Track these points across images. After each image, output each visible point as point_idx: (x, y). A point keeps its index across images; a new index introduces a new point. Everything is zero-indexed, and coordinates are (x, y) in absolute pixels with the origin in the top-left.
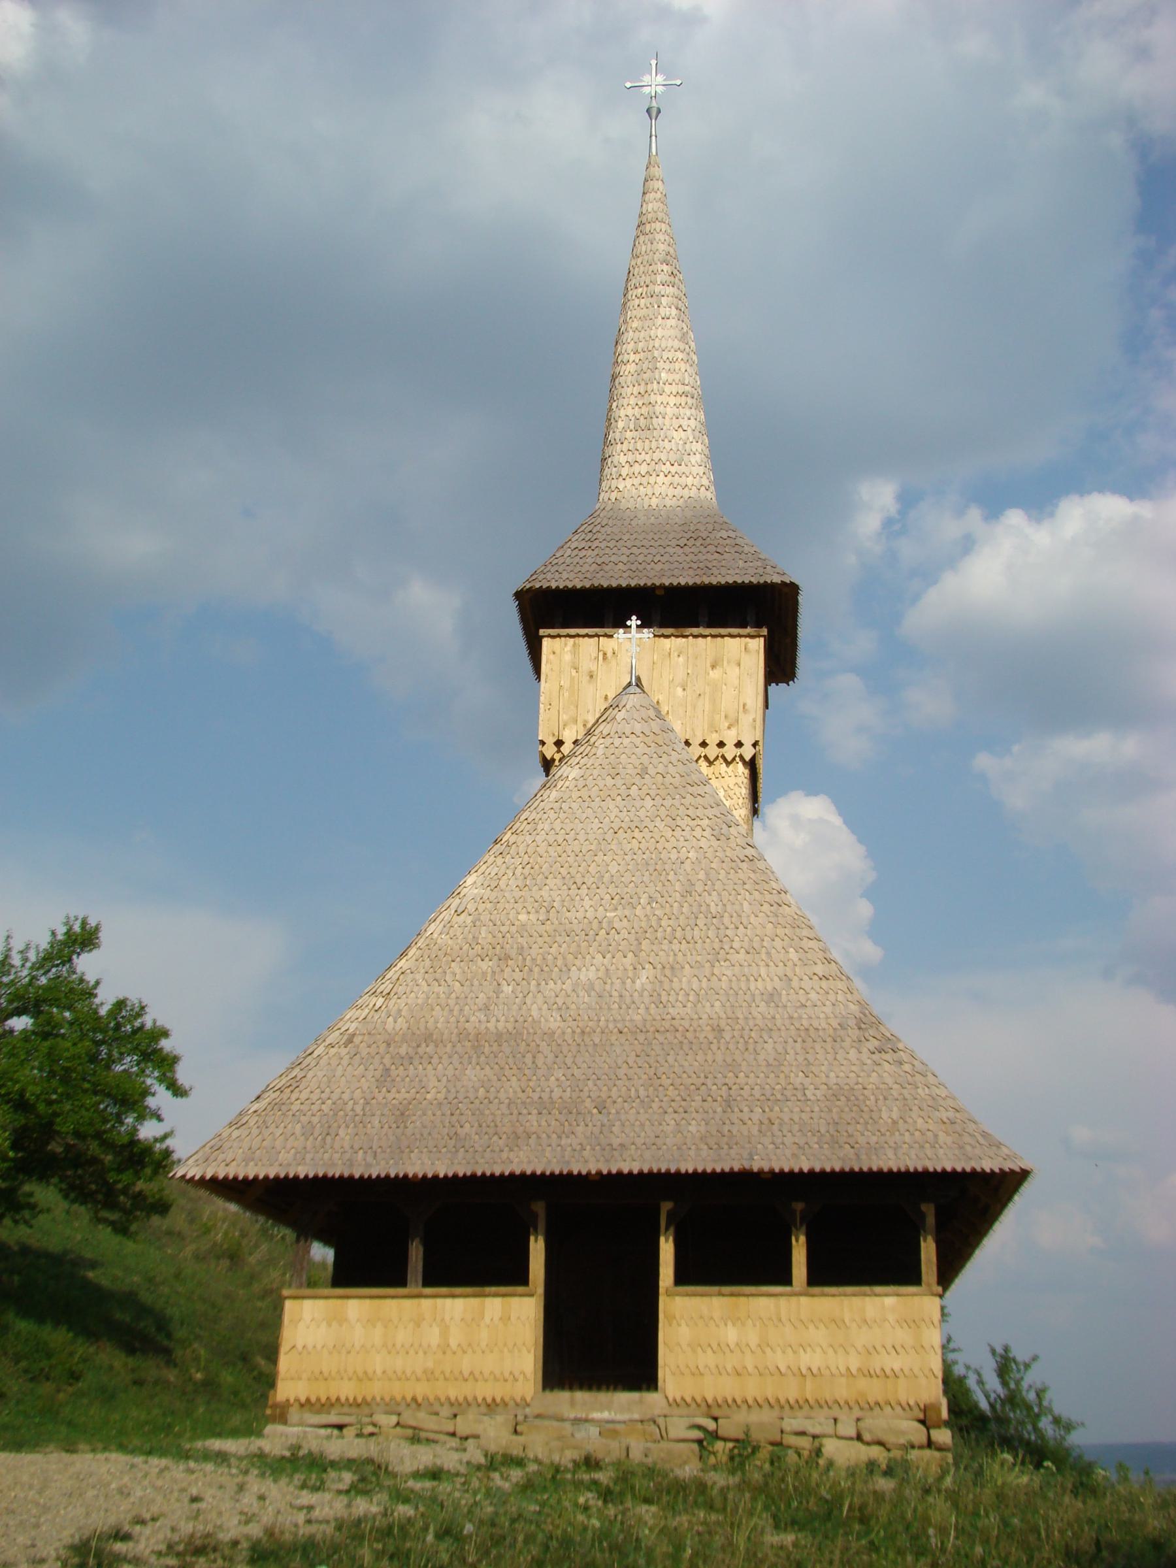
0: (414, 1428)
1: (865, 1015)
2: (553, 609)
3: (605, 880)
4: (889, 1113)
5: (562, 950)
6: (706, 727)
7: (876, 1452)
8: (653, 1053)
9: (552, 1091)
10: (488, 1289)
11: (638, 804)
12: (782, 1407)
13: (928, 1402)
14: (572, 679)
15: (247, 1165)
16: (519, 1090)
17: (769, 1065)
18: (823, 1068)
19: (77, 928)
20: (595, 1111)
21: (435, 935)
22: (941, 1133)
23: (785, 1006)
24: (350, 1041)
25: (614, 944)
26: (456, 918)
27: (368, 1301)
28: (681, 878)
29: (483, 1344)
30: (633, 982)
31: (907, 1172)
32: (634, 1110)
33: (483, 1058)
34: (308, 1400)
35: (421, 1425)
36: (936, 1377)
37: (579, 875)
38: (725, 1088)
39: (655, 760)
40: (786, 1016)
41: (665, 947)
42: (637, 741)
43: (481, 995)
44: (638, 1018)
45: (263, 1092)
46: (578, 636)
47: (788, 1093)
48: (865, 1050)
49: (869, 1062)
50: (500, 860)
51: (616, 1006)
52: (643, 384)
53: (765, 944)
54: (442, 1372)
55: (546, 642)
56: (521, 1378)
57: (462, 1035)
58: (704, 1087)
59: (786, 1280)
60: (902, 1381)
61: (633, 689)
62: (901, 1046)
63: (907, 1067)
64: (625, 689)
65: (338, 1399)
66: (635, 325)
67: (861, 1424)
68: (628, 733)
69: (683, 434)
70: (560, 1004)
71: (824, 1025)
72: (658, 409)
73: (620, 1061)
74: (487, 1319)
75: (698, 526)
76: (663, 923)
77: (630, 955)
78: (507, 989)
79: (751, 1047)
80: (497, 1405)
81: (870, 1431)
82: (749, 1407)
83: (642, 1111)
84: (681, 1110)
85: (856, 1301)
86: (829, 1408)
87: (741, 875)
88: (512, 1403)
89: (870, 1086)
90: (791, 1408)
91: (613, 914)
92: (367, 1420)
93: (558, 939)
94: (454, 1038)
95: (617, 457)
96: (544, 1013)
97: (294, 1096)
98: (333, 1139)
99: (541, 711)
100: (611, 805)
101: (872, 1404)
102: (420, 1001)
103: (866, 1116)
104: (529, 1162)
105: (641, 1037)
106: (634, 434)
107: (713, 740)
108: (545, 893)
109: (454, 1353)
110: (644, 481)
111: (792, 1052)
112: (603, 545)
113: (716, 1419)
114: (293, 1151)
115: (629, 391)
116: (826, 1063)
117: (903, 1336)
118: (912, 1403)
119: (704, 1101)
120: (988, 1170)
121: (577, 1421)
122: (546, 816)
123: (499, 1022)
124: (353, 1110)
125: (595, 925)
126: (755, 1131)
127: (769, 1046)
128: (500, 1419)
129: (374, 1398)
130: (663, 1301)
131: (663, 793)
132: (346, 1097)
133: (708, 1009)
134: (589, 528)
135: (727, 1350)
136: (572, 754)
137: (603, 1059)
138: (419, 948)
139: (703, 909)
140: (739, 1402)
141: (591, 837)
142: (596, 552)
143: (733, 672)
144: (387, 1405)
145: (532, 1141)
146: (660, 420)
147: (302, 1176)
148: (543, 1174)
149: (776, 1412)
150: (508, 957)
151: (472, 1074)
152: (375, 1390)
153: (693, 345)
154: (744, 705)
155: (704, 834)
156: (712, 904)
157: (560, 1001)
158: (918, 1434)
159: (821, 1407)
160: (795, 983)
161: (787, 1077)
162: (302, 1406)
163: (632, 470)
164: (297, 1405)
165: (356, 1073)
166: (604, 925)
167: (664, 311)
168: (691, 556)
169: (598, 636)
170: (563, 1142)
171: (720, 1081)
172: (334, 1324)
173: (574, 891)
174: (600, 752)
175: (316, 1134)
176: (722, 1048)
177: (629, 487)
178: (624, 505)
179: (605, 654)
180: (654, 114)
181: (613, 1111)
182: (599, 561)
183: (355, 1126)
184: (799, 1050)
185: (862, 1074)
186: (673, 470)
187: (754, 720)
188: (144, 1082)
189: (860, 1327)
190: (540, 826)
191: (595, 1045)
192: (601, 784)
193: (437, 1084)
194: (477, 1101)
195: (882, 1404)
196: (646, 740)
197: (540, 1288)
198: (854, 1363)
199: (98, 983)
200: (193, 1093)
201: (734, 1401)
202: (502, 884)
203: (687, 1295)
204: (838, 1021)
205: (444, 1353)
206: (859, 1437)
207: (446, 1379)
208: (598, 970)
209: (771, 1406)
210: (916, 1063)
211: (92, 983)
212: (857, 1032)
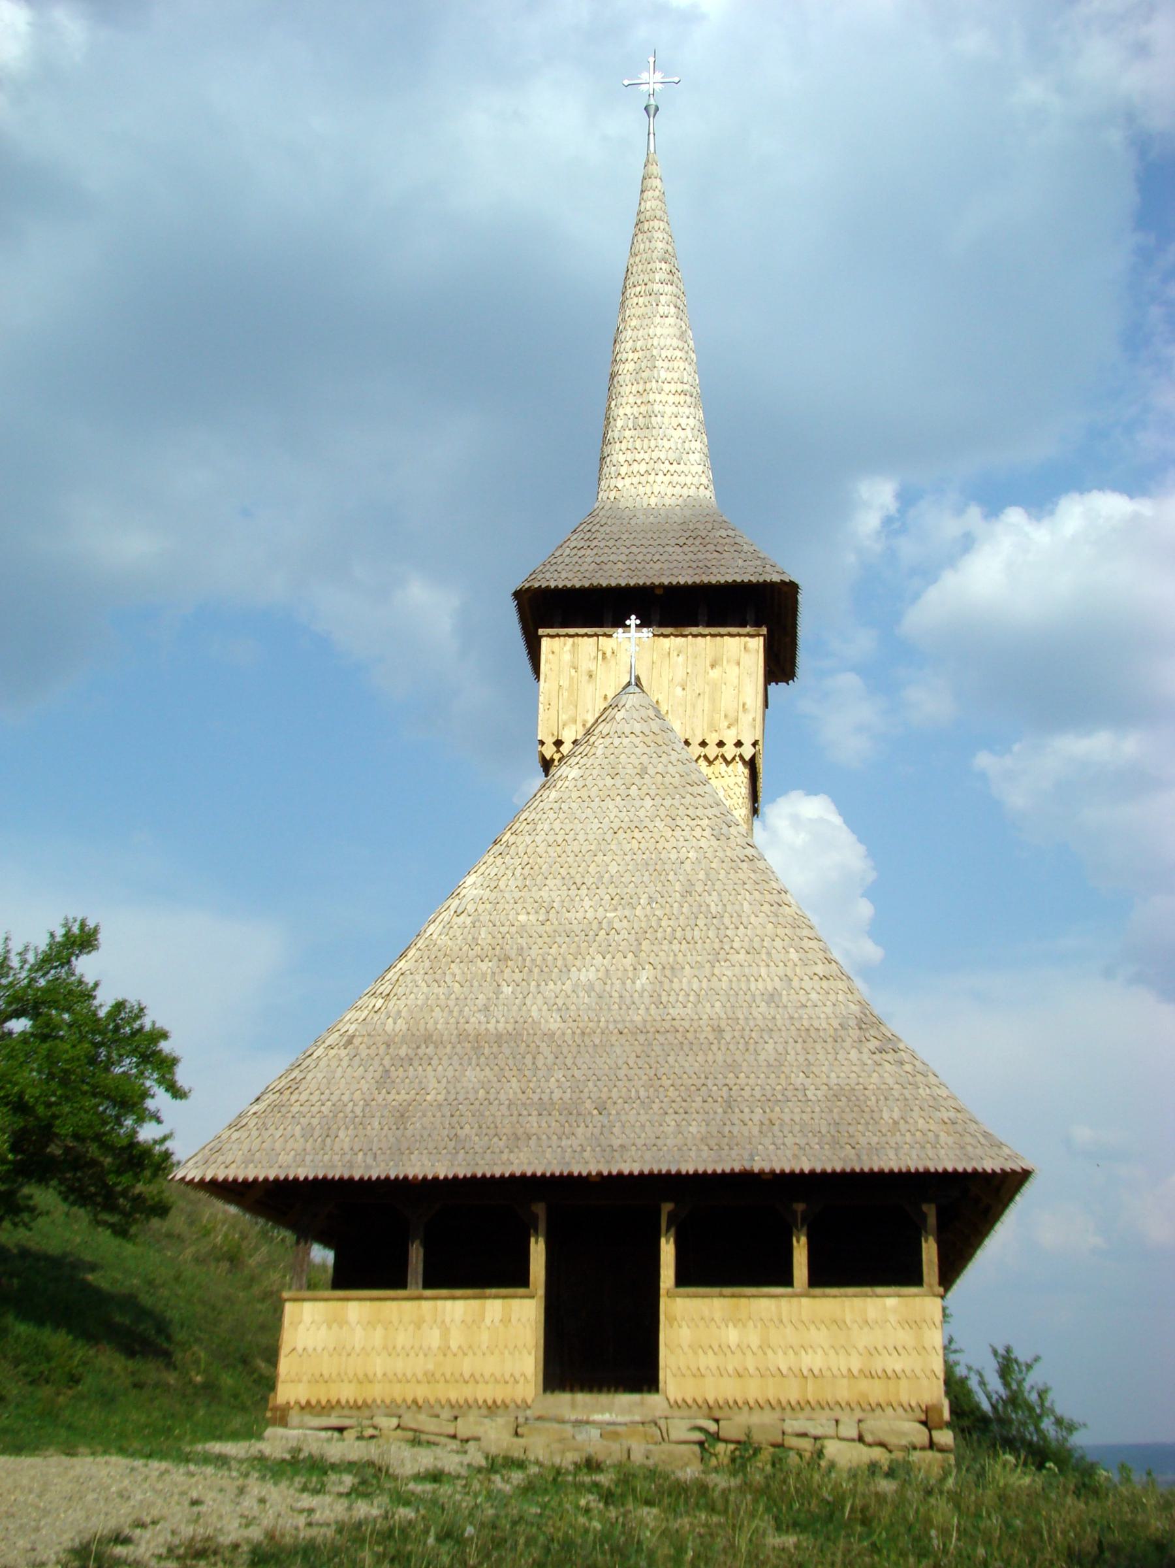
0: (415, 1431)
2: (551, 609)
5: (562, 951)
6: (705, 727)
7: (877, 1453)
8: (653, 1054)
10: (488, 1291)
11: (638, 803)
12: (784, 1409)
13: (930, 1403)
14: (572, 678)
15: (246, 1167)
17: (769, 1065)
18: (824, 1069)
19: (76, 929)
20: (595, 1112)
21: (435, 936)
22: (942, 1134)
23: (786, 1007)
24: (350, 1042)
25: (614, 944)
26: (455, 919)
27: (368, 1303)
28: (681, 878)
29: (484, 1347)
30: (634, 982)
31: (909, 1173)
32: (634, 1111)
33: (482, 1059)
34: (308, 1403)
35: (421, 1428)
36: (938, 1378)
37: (579, 875)
38: (725, 1088)
39: (655, 760)
40: (786, 1016)
41: (665, 947)
42: (637, 741)
43: (481, 996)
45: (263, 1094)
46: (577, 635)
47: (789, 1094)
48: (865, 1050)
49: (870, 1062)
50: (499, 861)
51: (616, 1006)
52: (641, 382)
54: (443, 1374)
55: (545, 642)
56: (522, 1380)
57: (462, 1036)
58: (704, 1088)
59: (786, 1280)
60: (904, 1383)
61: (632, 688)
62: (901, 1046)
63: (908, 1067)
64: (624, 688)
65: (338, 1402)
66: (634, 323)
68: (627, 732)
70: (560, 1005)
71: (824, 1025)
72: (657, 408)
73: (620, 1062)
74: (488, 1321)
75: (697, 525)
78: (507, 990)
79: (751, 1048)
80: (498, 1407)
81: (872, 1433)
82: (751, 1408)
83: (642, 1112)
84: (681, 1111)
86: (831, 1409)
88: (512, 1405)
89: (871, 1087)
91: (613, 915)
92: (367, 1422)
93: (558, 939)
94: (454, 1039)
95: (615, 456)
96: (544, 1014)
97: (294, 1097)
100: (611, 804)
101: (874, 1405)
102: (419, 1002)
103: (867, 1116)
104: (529, 1163)
105: (641, 1038)
106: (633, 432)
107: (712, 740)
108: (544, 893)
110: (643, 480)
113: (717, 1421)
114: (293, 1153)
115: (628, 389)
117: (904, 1337)
118: (913, 1404)
120: (989, 1171)
121: (578, 1423)
123: (499, 1023)
124: (352, 1111)
125: (595, 925)
126: (756, 1131)
127: (770, 1047)
128: (500, 1421)
129: (374, 1401)
130: (664, 1303)
131: (662, 792)
132: (345, 1098)
133: (708, 1009)
134: (588, 528)
136: (572, 754)
137: (603, 1059)
138: (419, 949)
139: (703, 909)
140: (740, 1403)
142: (595, 551)
143: (733, 671)
144: (388, 1407)
145: (533, 1142)
146: (659, 419)
147: (302, 1178)
149: (777, 1414)
150: (508, 958)
152: (376, 1392)
153: (691, 343)
154: (744, 705)
155: (704, 834)
156: (712, 904)
157: (560, 1002)
158: (919, 1435)
159: (823, 1408)
162: (302, 1408)
163: (631, 469)
164: (297, 1408)
165: (355, 1074)
166: (604, 925)
167: (661, 310)
168: (691, 555)
169: (597, 635)
170: (564, 1143)
171: (720, 1082)
172: (335, 1326)
173: (573, 892)
174: (599, 752)
175: (316, 1135)
176: (723, 1048)
178: (622, 504)
179: (604, 654)
180: (652, 112)
181: (614, 1112)
182: (598, 560)
183: (355, 1128)
185: (863, 1074)
187: (754, 720)
188: (143, 1084)
189: (861, 1328)
190: (539, 827)
192: (600, 783)
193: (437, 1085)
194: (477, 1103)
195: (884, 1405)
197: (541, 1291)
198: (856, 1364)
199: (96, 985)
200: (192, 1095)
201: (736, 1402)
202: (502, 884)
203: (688, 1296)
204: (839, 1021)
205: (445, 1355)
206: (861, 1439)
207: (446, 1381)
208: (598, 971)
209: (773, 1408)
211: (91, 985)
212: (858, 1032)
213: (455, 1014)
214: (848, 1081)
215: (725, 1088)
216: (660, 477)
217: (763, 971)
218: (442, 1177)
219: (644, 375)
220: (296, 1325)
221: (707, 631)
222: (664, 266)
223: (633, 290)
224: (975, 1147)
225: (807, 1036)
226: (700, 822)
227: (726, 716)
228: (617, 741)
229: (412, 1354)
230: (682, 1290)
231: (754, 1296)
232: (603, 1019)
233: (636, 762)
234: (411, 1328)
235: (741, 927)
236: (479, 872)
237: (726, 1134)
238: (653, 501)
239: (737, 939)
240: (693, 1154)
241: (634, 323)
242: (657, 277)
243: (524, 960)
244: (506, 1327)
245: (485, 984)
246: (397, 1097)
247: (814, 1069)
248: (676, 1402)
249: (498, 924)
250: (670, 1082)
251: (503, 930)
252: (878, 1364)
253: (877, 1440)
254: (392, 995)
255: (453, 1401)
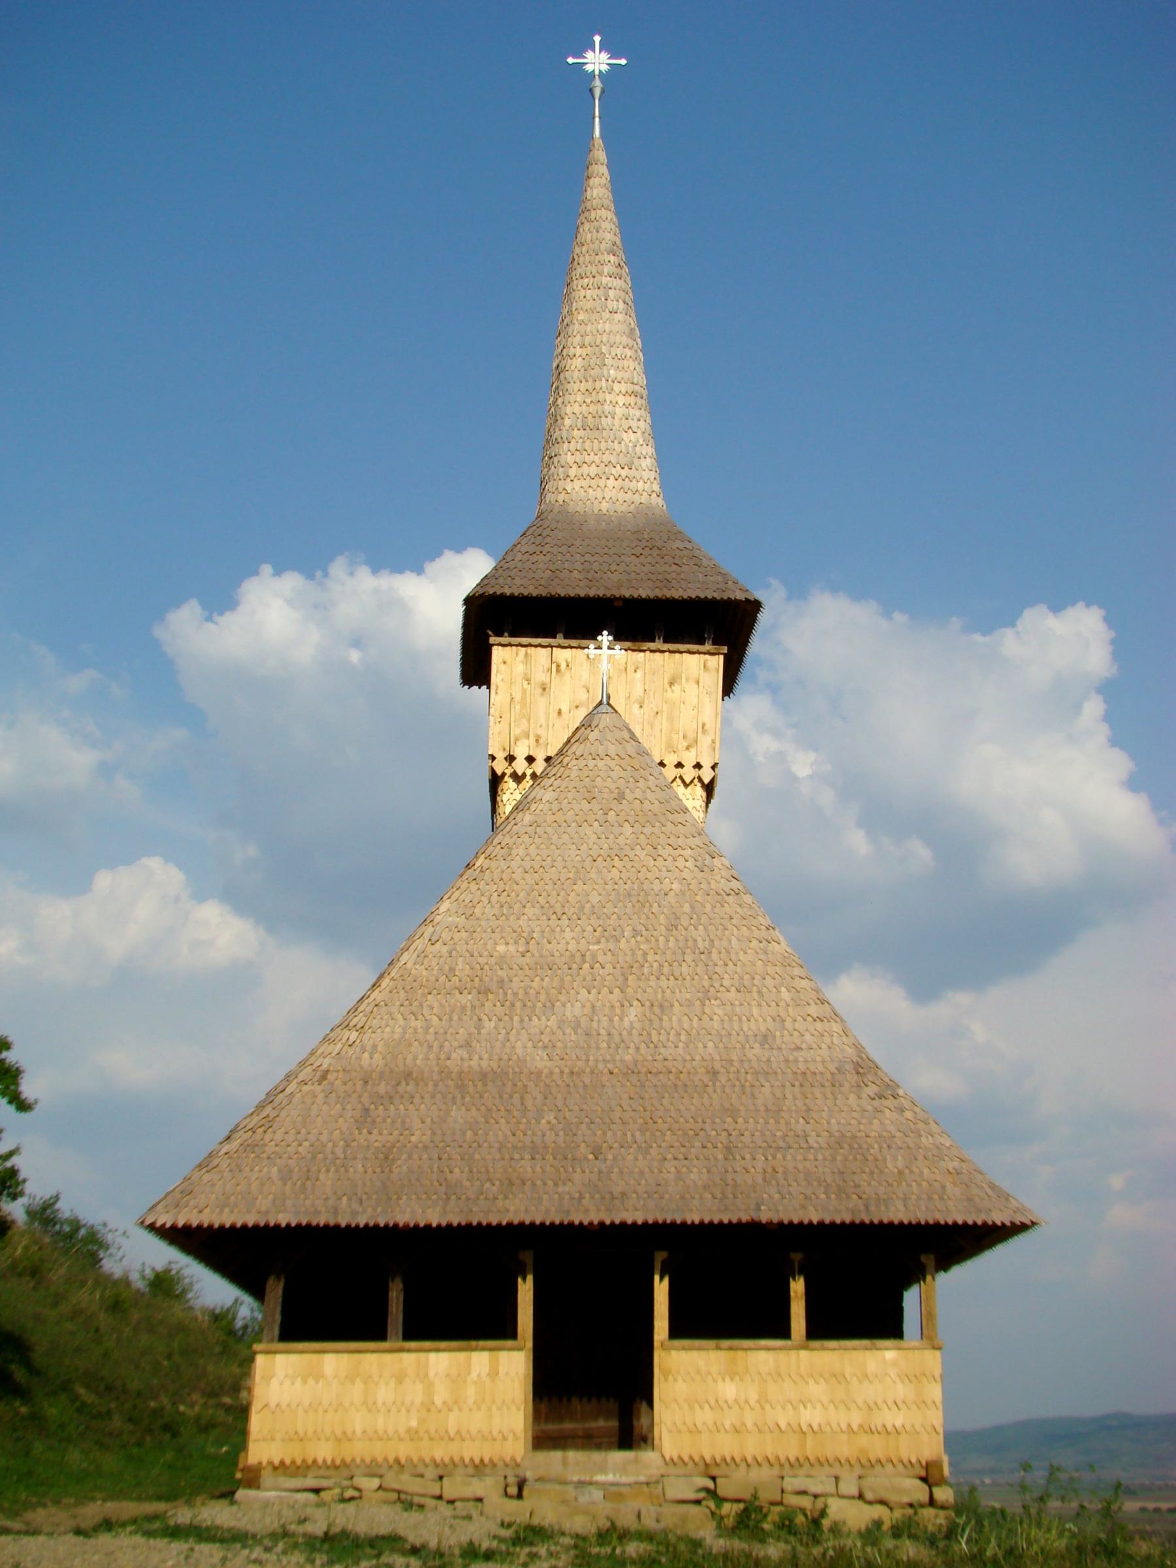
0: (399, 1492)
1: (862, 1059)
3: (586, 911)
4: (894, 1163)
5: (545, 984)
6: (663, 747)
7: (879, 1511)
8: (647, 1096)
9: (544, 1135)
11: (617, 830)
12: (782, 1466)
14: (524, 691)
15: (222, 1212)
16: (509, 1133)
17: (767, 1110)
18: (824, 1114)
20: (591, 1156)
21: (409, 965)
22: (948, 1184)
23: (780, 1049)
24: (324, 1077)
25: (598, 978)
26: (430, 948)
27: (345, 1356)
28: (665, 910)
29: (470, 1402)
30: (621, 1019)
33: (468, 1099)
34: (282, 1463)
35: (405, 1488)
36: (937, 1433)
37: (558, 905)
40: (782, 1058)
41: (652, 983)
42: (612, 764)
43: (461, 1031)
44: (628, 1058)
46: (530, 645)
47: (790, 1140)
48: (864, 1096)
49: (869, 1108)
50: (473, 886)
51: (605, 1045)
52: (590, 380)
53: (756, 982)
54: (427, 1431)
55: (497, 654)
56: (511, 1437)
57: (445, 1073)
58: (702, 1133)
59: (781, 1330)
61: (604, 708)
62: (901, 1092)
63: (908, 1114)
64: (596, 708)
65: (315, 1461)
66: (581, 317)
67: (864, 1482)
68: (602, 755)
69: (633, 437)
72: (607, 408)
74: (474, 1375)
76: (650, 958)
77: (617, 991)
78: (489, 1025)
79: (748, 1090)
82: (748, 1465)
83: (640, 1157)
84: (681, 1156)
85: (859, 1355)
86: (830, 1465)
87: (727, 908)
88: (500, 1464)
89: (873, 1134)
90: (791, 1466)
91: (596, 947)
92: (347, 1483)
93: (539, 972)
94: (436, 1077)
95: (563, 456)
96: (529, 1051)
97: (268, 1136)
98: (314, 1185)
99: (492, 723)
100: (589, 831)
101: (873, 1462)
102: (396, 1036)
104: (526, 1210)
105: (634, 1079)
107: (670, 760)
108: (523, 922)
109: (440, 1411)
110: (593, 483)
111: (790, 1096)
112: (555, 550)
113: (714, 1479)
114: (271, 1197)
115: (576, 386)
116: (826, 1109)
117: (902, 1391)
118: (914, 1460)
119: (704, 1147)
120: (999, 1224)
121: (581, 1484)
122: (520, 840)
124: (333, 1153)
125: (578, 959)
127: (767, 1090)
128: (489, 1481)
129: (353, 1460)
132: (324, 1138)
133: (701, 1050)
134: (539, 531)
135: (725, 1406)
136: (545, 775)
138: (392, 979)
139: (690, 943)
140: (738, 1460)
141: (569, 865)
143: (692, 691)
144: (368, 1466)
145: (527, 1188)
146: (609, 420)
148: (543, 1224)
149: (776, 1471)
150: (488, 991)
151: (458, 1115)
152: (359, 1451)
153: (639, 340)
155: (687, 864)
156: (699, 939)
157: (545, 1038)
158: (920, 1492)
160: (788, 1024)
161: (788, 1123)
162: (275, 1468)
163: (581, 470)
164: (270, 1468)
165: (332, 1112)
166: (588, 958)
167: (612, 305)
170: (560, 1189)
172: (311, 1381)
173: (553, 922)
174: (574, 774)
175: (295, 1177)
176: (719, 1091)
177: (577, 488)
178: (571, 508)
179: (558, 666)
181: (610, 1157)
183: (337, 1171)
184: (798, 1095)
186: (624, 473)
187: (713, 742)
189: (860, 1382)
190: (514, 852)
191: (585, 1086)
192: (577, 807)
193: (421, 1125)
196: (622, 762)
197: (530, 1344)
198: (856, 1419)
201: (733, 1459)
202: (478, 911)
203: (683, 1349)
204: (836, 1064)
205: (429, 1411)
206: (861, 1496)
207: (431, 1439)
208: (583, 1006)
209: (771, 1465)
210: (917, 1110)
212: (856, 1077)
213: (435, 1049)
214: (849, 1128)
215: (724, 1134)
216: (611, 482)
217: (755, 1011)
218: (434, 1225)
219: (592, 373)
220: (268, 1378)
221: (666, 646)
222: (612, 258)
223: (581, 282)
224: (982, 1199)
225: (804, 1079)
226: (682, 852)
227: (684, 737)
228: (591, 763)
229: (394, 1409)
230: (677, 1343)
231: (751, 1349)
232: (591, 1058)
233: (613, 786)
234: (393, 1382)
235: (730, 964)
236: (454, 897)
237: (730, 1182)
238: (605, 506)
239: (726, 976)
240: (696, 1202)
241: (581, 317)
242: (606, 270)
243: (506, 994)
244: (493, 1381)
245: (465, 1018)
246: (379, 1138)
247: (815, 1115)
248: (672, 1459)
249: (476, 954)
250: (667, 1126)
251: (480, 960)
252: (877, 1421)
253: (878, 1497)
254: (366, 1027)
255: (438, 1459)
